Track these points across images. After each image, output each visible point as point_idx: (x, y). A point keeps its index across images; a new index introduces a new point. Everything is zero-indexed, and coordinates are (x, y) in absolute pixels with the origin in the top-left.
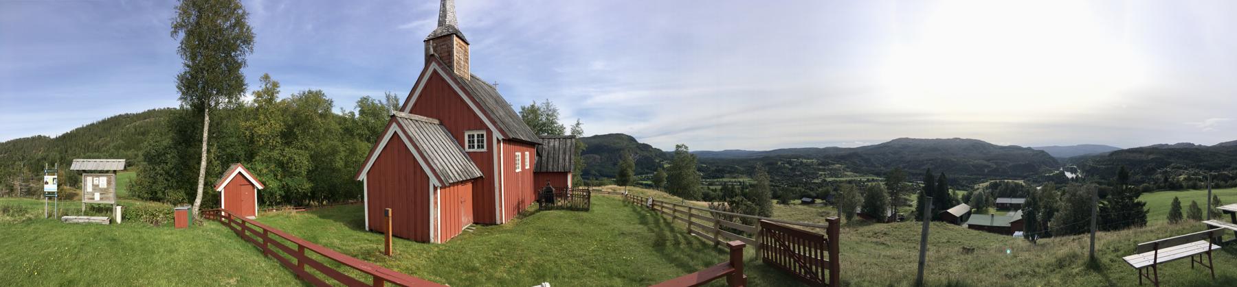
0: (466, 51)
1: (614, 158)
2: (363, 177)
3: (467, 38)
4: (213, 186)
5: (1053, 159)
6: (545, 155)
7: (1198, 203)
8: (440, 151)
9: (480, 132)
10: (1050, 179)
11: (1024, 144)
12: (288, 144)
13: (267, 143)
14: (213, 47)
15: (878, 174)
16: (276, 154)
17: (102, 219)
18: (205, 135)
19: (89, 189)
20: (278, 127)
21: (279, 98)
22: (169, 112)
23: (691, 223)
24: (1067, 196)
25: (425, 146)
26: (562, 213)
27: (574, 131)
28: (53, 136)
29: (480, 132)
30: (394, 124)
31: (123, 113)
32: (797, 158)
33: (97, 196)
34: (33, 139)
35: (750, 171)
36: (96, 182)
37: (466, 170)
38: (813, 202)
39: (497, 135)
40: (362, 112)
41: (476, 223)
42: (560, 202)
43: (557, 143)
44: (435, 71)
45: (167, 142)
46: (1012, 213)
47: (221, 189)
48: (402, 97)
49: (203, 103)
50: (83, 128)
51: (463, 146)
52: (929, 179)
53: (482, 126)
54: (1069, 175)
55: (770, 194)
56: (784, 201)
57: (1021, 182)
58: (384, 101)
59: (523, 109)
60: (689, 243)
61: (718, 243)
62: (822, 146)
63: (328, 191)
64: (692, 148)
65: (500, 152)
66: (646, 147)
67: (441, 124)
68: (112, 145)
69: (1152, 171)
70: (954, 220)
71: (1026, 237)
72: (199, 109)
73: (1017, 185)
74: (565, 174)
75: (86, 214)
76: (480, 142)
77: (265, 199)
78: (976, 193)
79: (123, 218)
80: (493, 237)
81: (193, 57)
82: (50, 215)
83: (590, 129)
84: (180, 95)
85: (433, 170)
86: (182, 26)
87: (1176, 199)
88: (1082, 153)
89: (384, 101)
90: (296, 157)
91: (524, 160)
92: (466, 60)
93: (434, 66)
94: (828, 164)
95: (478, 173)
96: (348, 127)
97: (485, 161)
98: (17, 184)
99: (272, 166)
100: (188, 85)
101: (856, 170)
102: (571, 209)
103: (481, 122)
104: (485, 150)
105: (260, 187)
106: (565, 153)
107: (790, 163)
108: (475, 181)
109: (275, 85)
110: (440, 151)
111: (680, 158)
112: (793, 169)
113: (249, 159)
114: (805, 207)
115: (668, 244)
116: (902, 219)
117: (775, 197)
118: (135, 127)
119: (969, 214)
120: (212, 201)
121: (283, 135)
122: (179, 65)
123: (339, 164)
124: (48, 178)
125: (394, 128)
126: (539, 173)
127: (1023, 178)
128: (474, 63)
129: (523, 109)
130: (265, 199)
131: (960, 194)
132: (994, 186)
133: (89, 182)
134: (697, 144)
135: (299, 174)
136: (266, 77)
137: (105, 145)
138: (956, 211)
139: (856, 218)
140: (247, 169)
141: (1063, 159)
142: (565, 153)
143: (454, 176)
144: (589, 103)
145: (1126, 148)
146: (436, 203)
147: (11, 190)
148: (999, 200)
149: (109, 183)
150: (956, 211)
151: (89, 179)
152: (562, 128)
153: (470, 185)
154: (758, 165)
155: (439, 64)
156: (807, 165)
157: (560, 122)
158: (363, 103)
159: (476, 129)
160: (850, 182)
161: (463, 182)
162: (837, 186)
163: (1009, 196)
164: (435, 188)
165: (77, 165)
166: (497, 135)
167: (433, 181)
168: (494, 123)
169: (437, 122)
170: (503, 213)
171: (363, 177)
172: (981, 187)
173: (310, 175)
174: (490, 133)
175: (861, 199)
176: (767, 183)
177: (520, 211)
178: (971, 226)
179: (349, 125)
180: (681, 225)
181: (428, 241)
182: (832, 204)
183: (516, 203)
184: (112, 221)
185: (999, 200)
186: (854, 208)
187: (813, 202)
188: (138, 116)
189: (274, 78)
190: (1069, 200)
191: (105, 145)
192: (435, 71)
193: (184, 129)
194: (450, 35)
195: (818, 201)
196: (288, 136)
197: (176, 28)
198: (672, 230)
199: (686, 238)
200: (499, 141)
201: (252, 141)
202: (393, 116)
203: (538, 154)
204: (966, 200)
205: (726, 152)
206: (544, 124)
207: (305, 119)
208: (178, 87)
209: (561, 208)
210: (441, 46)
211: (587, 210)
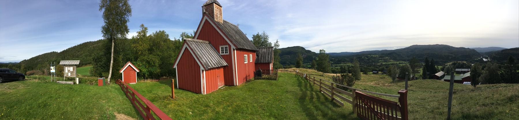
0: (220, 10)
1: (295, 57)
2: (175, 66)
3: (222, 5)
4: (119, 70)
6: (260, 55)
8: (207, 56)
9: (226, 46)
10: (477, 61)
12: (151, 53)
14: (116, 15)
15: (405, 61)
16: (145, 58)
17: (71, 82)
18: (113, 50)
19: (67, 71)
20: (146, 46)
21: (148, 35)
22: (100, 41)
23: (321, 87)
24: (486, 68)
26: (263, 81)
27: (275, 45)
28: (59, 52)
29: (226, 46)
30: (185, 44)
31: (89, 41)
33: (69, 74)
35: (351, 61)
38: (378, 73)
39: (233, 47)
41: (226, 85)
42: (264, 76)
43: (265, 50)
44: (206, 20)
45: (102, 53)
46: (462, 75)
47: (122, 72)
48: (191, 31)
49: (111, 37)
50: (71, 48)
51: (219, 53)
52: (427, 61)
53: (227, 43)
54: (485, 60)
55: (359, 70)
56: (365, 73)
57: (465, 62)
59: (254, 36)
60: (319, 98)
61: (333, 99)
63: (162, 73)
64: (327, 51)
66: (309, 51)
67: (210, 43)
71: (472, 84)
72: (110, 40)
73: (463, 63)
75: (65, 80)
77: (141, 76)
78: (447, 67)
79: (80, 82)
80: (232, 91)
81: (108, 19)
82: (53, 81)
83: (283, 45)
84: (103, 35)
86: (104, 6)
88: (490, 51)
91: (249, 59)
92: (221, 14)
93: (206, 17)
94: (383, 57)
95: (225, 64)
97: (228, 58)
98: (45, 70)
99: (144, 63)
100: (106, 30)
101: (395, 59)
102: (268, 79)
103: (226, 41)
104: (228, 54)
105: (138, 71)
106: (268, 55)
107: (367, 57)
108: (224, 67)
109: (146, 29)
110: (207, 56)
111: (322, 56)
112: (369, 60)
113: (134, 59)
114: (375, 75)
115: (307, 98)
116: (417, 79)
117: (361, 71)
119: (444, 76)
120: (116, 77)
121: (149, 50)
122: (102, 23)
125: (186, 45)
126: (257, 64)
127: (466, 61)
129: (254, 36)
130: (141, 76)
131: (440, 67)
132: (454, 64)
133: (66, 69)
134: (329, 50)
135: (155, 66)
136: (142, 26)
137: (81, 55)
138: (439, 74)
139: (397, 79)
140: (133, 64)
141: (482, 53)
142: (268, 55)
146: (203, 77)
147: (44, 73)
148: (457, 70)
149: (74, 69)
150: (439, 74)
151: (66, 68)
152: (270, 44)
153: (222, 69)
155: (208, 17)
156: (375, 58)
158: (183, 35)
159: (224, 45)
160: (392, 64)
161: (218, 68)
162: (387, 66)
163: (460, 68)
164: (203, 71)
165: (62, 63)
166: (233, 47)
167: (202, 68)
168: (231, 42)
169: (207, 42)
170: (237, 81)
171: (175, 66)
172: (449, 64)
175: (398, 71)
176: (358, 65)
177: (247, 80)
178: (445, 80)
179: (178, 45)
180: (317, 87)
181: (201, 93)
182: (385, 73)
183: (245, 76)
184: (75, 83)
185: (457, 70)
186: (395, 75)
187: (378, 73)
189: (145, 26)
190: (487, 70)
191: (81, 55)
192: (206, 20)
193: (105, 47)
194: (212, 3)
195: (380, 72)
196: (151, 50)
197: (101, 7)
198: (312, 90)
199: (317, 95)
200: (234, 50)
201: (137, 53)
202: (185, 40)
203: (257, 55)
204: (442, 70)
206: (263, 43)
208: (102, 32)
209: (264, 79)
210: (208, 10)
211: (275, 79)
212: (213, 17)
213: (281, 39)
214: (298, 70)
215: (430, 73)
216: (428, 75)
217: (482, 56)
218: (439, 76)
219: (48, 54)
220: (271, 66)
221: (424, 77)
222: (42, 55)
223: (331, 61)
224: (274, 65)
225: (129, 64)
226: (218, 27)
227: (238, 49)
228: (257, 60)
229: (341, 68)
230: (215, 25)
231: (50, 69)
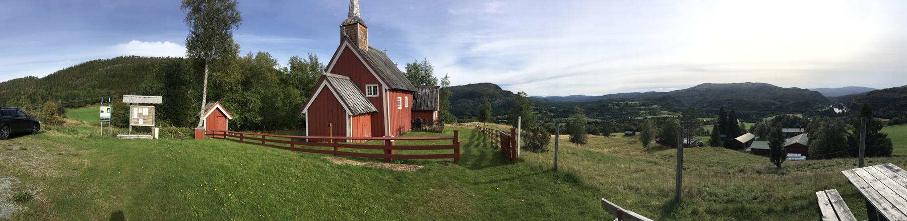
2: (305, 111)
6: (419, 99)
8: (351, 96)
13: (231, 89)
16: (237, 96)
18: (206, 82)
25: (342, 93)
28: (40, 77)
34: (26, 78)
36: (140, 112)
37: (366, 107)
38: (633, 134)
39: (384, 87)
40: (293, 68)
44: (347, 47)
48: (324, 60)
50: (63, 71)
51: (365, 93)
52: (722, 114)
53: (376, 82)
54: (837, 110)
58: (308, 61)
59: (408, 65)
65: (387, 97)
67: (351, 80)
68: (87, 84)
70: (740, 146)
73: (796, 118)
74: (432, 111)
76: (375, 90)
85: (348, 107)
88: (847, 93)
89: (308, 61)
90: (252, 99)
91: (404, 102)
92: (366, 39)
93: (346, 43)
94: (648, 105)
95: (374, 109)
96: (283, 79)
97: (378, 102)
108: (372, 114)
110: (351, 96)
112: (621, 110)
118: (107, 71)
121: (243, 83)
123: (279, 104)
125: (325, 83)
126: (415, 111)
127: (801, 113)
128: (368, 41)
129: (408, 65)
131: (748, 126)
138: (742, 139)
140: (224, 107)
144: (474, 51)
150: (742, 139)
152: (435, 80)
153: (369, 116)
154: (577, 108)
155: (350, 43)
156: (632, 106)
159: (372, 83)
165: (127, 99)
166: (384, 87)
167: (348, 112)
168: (383, 79)
171: (305, 111)
173: (262, 111)
174: (381, 86)
187: (633, 134)
188: (108, 62)
191: (82, 84)
192: (347, 47)
194: (356, 24)
196: (246, 84)
204: (751, 131)
205: (570, 97)
206: (423, 77)
207: (257, 72)
209: (425, 131)
212: (357, 43)
213: (450, 72)
214: (481, 125)
215: (725, 136)
216: (723, 139)
217: (833, 104)
218: (743, 142)
219: (21, 80)
220: (435, 116)
221: (714, 143)
222: (9, 82)
223: (551, 111)
224: (439, 112)
225: (218, 106)
226: (364, 58)
227: (392, 90)
228: (415, 105)
229: (568, 124)
230: (361, 55)
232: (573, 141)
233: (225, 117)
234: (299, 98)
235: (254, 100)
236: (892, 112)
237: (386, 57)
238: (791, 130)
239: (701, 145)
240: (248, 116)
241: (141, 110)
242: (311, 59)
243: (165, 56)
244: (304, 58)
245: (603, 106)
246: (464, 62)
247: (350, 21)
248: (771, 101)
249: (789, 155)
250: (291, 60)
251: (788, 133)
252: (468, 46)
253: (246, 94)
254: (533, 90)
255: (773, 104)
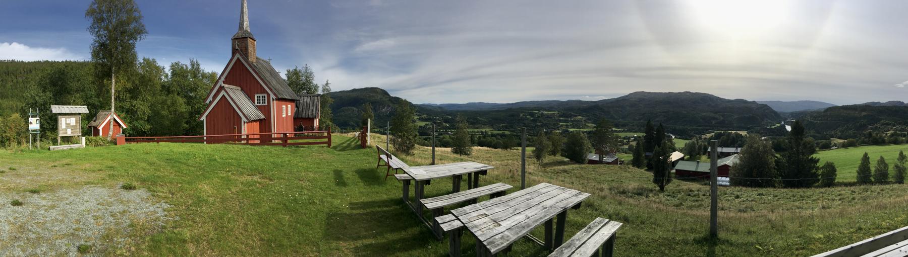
2: (204, 118)
5: (775, 113)
6: (301, 107)
7: (885, 158)
8: (246, 107)
11: (749, 99)
32: (539, 109)
39: (272, 96)
44: (238, 59)
53: (265, 91)
58: (190, 67)
62: (564, 99)
65: (274, 105)
66: (397, 100)
67: (242, 90)
69: (863, 127)
74: (313, 119)
87: (866, 154)
91: (288, 110)
93: (237, 56)
94: (571, 116)
95: (263, 117)
97: (266, 110)
108: (261, 121)
110: (246, 107)
112: (535, 121)
124: (31, 119)
125: (223, 93)
128: (258, 52)
132: (718, 136)
133: (63, 122)
140: (119, 116)
141: (785, 113)
143: (253, 118)
145: (841, 105)
149: (76, 122)
152: (316, 87)
156: (548, 117)
157: (315, 82)
161: (255, 121)
165: (55, 109)
166: (272, 96)
167: (244, 119)
168: (271, 90)
171: (204, 118)
174: (269, 95)
206: (304, 84)
212: (247, 56)
217: (785, 120)
220: (316, 123)
223: (446, 121)
227: (278, 99)
228: (297, 113)
231: (27, 123)
232: (455, 152)
233: (119, 125)
234: (184, 106)
235: (143, 107)
236: (851, 132)
237: (270, 66)
238: (725, 150)
239: (622, 163)
240: (136, 124)
241: (68, 120)
242: (193, 65)
243: (45, 60)
244: (186, 62)
245: (513, 116)
246: (349, 64)
247: (240, 34)
248: (712, 115)
249: (719, 178)
250: (173, 66)
251: (722, 153)
252: (353, 44)
253: (134, 103)
254: (417, 97)
255: (714, 118)
